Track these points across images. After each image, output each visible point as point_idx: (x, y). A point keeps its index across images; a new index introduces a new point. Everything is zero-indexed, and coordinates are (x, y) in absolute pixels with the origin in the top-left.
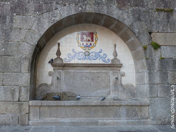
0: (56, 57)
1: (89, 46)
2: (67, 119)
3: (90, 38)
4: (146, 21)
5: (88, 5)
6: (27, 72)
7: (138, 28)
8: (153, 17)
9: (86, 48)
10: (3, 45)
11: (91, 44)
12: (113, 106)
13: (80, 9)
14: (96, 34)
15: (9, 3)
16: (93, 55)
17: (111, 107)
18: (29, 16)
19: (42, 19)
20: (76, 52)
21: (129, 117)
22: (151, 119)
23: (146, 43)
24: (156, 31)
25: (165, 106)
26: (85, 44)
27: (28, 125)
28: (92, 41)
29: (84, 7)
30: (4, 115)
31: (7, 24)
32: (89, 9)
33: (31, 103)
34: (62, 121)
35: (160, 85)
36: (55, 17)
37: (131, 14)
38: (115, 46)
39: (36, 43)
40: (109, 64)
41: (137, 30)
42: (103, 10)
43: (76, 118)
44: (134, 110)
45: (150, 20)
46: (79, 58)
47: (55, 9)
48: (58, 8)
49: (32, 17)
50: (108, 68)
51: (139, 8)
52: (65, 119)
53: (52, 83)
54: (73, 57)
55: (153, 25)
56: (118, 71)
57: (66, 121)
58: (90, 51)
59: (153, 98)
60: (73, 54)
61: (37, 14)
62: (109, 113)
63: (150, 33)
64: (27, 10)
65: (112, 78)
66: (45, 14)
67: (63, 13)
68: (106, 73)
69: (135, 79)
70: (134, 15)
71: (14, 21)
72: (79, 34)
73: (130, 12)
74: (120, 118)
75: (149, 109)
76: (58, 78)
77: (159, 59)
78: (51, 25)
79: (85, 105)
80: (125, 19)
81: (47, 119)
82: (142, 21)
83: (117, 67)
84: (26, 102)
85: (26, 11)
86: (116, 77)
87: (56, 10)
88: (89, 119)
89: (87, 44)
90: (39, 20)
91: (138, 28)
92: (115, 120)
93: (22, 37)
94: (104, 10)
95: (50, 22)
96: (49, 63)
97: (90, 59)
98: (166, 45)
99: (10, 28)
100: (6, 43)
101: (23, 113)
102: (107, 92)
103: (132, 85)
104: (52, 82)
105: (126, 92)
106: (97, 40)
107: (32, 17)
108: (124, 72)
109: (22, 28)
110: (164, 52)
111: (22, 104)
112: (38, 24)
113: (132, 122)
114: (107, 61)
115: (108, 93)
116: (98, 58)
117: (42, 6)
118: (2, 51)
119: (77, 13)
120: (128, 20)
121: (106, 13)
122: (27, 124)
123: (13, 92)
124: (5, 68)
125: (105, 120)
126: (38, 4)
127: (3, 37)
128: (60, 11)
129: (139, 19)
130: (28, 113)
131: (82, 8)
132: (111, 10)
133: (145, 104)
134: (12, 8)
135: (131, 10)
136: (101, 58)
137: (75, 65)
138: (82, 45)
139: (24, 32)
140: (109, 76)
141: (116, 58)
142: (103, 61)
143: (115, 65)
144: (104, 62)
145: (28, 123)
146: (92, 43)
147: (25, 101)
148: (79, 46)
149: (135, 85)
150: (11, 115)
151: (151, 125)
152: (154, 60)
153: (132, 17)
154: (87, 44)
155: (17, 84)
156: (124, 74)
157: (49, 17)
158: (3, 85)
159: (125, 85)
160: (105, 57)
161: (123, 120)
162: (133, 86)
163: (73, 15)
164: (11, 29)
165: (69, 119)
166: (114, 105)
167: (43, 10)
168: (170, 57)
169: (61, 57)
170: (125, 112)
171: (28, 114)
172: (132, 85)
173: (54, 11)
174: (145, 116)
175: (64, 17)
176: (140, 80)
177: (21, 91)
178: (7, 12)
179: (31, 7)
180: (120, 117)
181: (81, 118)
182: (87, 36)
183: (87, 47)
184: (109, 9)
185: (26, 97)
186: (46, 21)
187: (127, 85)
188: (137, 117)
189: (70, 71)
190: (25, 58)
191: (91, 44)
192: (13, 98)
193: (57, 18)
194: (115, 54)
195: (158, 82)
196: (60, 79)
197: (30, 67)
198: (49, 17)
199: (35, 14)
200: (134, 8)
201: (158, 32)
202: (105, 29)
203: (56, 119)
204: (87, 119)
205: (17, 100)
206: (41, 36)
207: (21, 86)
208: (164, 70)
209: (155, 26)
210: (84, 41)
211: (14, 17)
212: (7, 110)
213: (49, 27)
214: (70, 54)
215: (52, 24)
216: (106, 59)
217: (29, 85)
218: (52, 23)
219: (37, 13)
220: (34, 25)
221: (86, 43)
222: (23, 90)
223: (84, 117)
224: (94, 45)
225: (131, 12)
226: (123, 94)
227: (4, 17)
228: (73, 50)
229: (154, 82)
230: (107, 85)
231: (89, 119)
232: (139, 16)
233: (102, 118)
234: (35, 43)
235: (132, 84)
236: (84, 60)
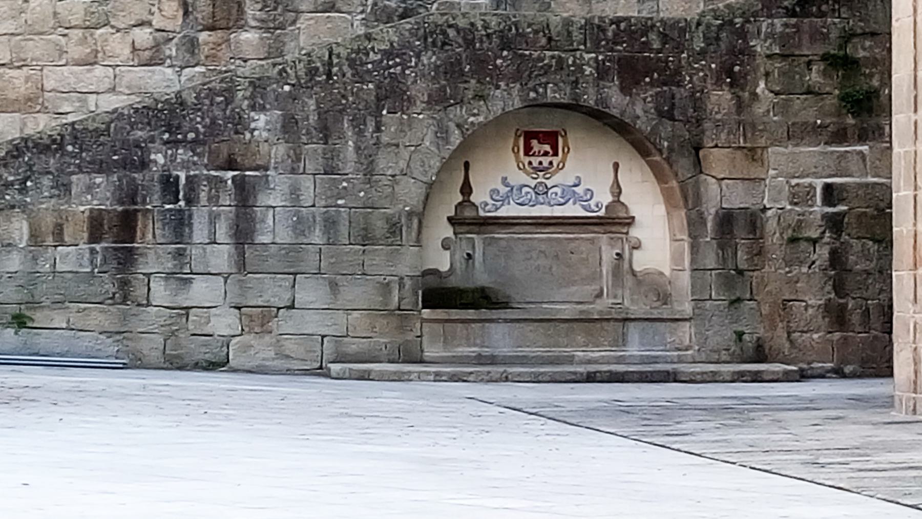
0: (460, 198)
5: (551, 85)
11: (551, 163)
12: (608, 320)
13: (532, 95)
14: (566, 134)
15: (371, 86)
16: (556, 194)
17: (605, 324)
20: (512, 184)
24: (711, 145)
28: (553, 155)
29: (541, 90)
33: (426, 313)
36: (474, 115)
37: (651, 105)
38: (616, 166)
41: (666, 144)
50: (596, 229)
54: (505, 200)
56: (624, 236)
58: (549, 183)
60: (504, 190)
65: (608, 255)
68: (592, 241)
69: (668, 256)
72: (520, 136)
73: (649, 99)
76: (468, 255)
80: (638, 117)
81: (460, 349)
83: (620, 224)
85: (409, 101)
86: (618, 251)
89: (541, 163)
96: (735, 332)
102: (595, 290)
103: (661, 274)
105: (642, 290)
107: (422, 117)
108: (639, 237)
116: (571, 201)
123: (386, 288)
131: (537, 92)
135: (651, 96)
136: (578, 199)
137: (511, 221)
140: (600, 248)
141: (619, 201)
143: (616, 221)
146: (556, 161)
149: (667, 273)
154: (541, 163)
156: (640, 243)
160: (589, 197)
164: (377, 144)
168: (742, 206)
169: (472, 198)
176: (676, 258)
182: (540, 143)
187: (647, 273)
189: (496, 236)
191: (551, 163)
194: (617, 190)
201: (716, 146)
210: (533, 155)
211: (383, 119)
214: (495, 191)
216: (592, 203)
228: (504, 180)
236: (533, 206)
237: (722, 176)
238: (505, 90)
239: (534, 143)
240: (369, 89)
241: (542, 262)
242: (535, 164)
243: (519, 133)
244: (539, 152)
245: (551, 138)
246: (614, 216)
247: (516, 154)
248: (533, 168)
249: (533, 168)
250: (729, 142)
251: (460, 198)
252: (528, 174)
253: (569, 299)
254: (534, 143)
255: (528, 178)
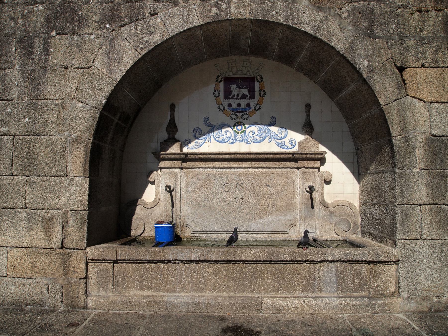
0: (166, 136)
1: (245, 109)
2: (182, 294)
3: (245, 91)
4: (389, 38)
6: (82, 175)
7: (369, 56)
8: (407, 26)
9: (238, 114)
10: (25, 109)
11: (248, 105)
15: (41, 7)
16: (254, 132)
17: (297, 266)
18: (86, 36)
19: (118, 41)
21: (344, 292)
22: (403, 299)
23: (388, 96)
25: (440, 264)
26: (234, 106)
27: (85, 307)
29: (224, 6)
30: (30, 280)
31: (36, 57)
32: (236, 11)
34: (171, 300)
35: (427, 207)
36: (150, 34)
37: (348, 21)
38: (308, 107)
39: (104, 102)
40: (293, 154)
41: (366, 63)
42: (274, 12)
43: (206, 292)
44: (358, 274)
45: (399, 35)
46: (221, 138)
47: (152, 15)
48: (158, 11)
49: (93, 36)
51: (369, 4)
52: (177, 294)
53: (155, 198)
55: (407, 49)
57: (179, 300)
59: (409, 242)
61: (108, 29)
62: (291, 282)
63: (401, 69)
64: (82, 22)
66: (126, 27)
67: (172, 23)
68: (286, 176)
70: (355, 23)
71: (52, 50)
72: (220, 82)
73: (345, 15)
74: (320, 294)
75: (397, 271)
77: (426, 139)
78: (139, 54)
79: (226, 259)
80: (334, 34)
81: (132, 293)
82: (380, 38)
84: (80, 252)
87: (152, 18)
88: (239, 295)
89: (239, 105)
90: (112, 42)
91: (367, 57)
92: (307, 301)
93: (70, 87)
94: (277, 13)
95: (138, 46)
97: (248, 143)
98: (443, 100)
99: (42, 67)
100: (32, 105)
101: (74, 278)
104: (156, 196)
106: (264, 96)
109: (70, 65)
110: (438, 119)
111: (69, 256)
112: (109, 54)
113: (353, 305)
114: (287, 144)
115: (291, 223)
116: (267, 138)
117: (118, 10)
118: (23, 125)
119: (205, 21)
120: (342, 35)
121: (281, 19)
122: (82, 304)
124: (29, 166)
125: (280, 300)
126: (110, 5)
127: (26, 91)
128: (164, 20)
129: (370, 34)
130: (84, 278)
131: (220, 9)
132: (294, 11)
133: (389, 259)
134: (47, 20)
138: (226, 108)
139: (73, 74)
142: (279, 145)
144: (281, 147)
145: (85, 303)
146: (253, 103)
147: (77, 249)
148: (220, 110)
150: (46, 282)
151: (402, 312)
152: (413, 140)
153: (350, 28)
154: (239, 105)
155: (59, 206)
157: (136, 35)
158: (26, 208)
159: (332, 203)
160: (283, 135)
161: (327, 300)
162: (353, 205)
163: (196, 28)
165: (186, 294)
166: (305, 261)
167: (121, 18)
170: (333, 279)
171: (85, 280)
172: (350, 204)
173: (148, 21)
174: (387, 288)
175: (173, 34)
177: (67, 222)
178: (37, 29)
179: (92, 12)
180: (321, 291)
181: (219, 292)
182: (238, 87)
183: (239, 112)
184: (291, 9)
185: (78, 238)
186: (128, 46)
188: (364, 291)
190: (77, 140)
191: (248, 105)
192: (48, 241)
193: (156, 36)
195: (424, 199)
196: (174, 189)
197: (88, 162)
198: (136, 35)
199: (101, 31)
200: (356, 4)
201: (423, 66)
202: (285, 68)
203: (155, 294)
204: (232, 294)
205: (58, 244)
206: (116, 83)
207: (68, 209)
208: (439, 167)
209: (412, 51)
210: (232, 98)
212: (35, 269)
213: (136, 59)
215: (143, 53)
217: (86, 207)
218: (142, 49)
219: (108, 26)
220: (98, 59)
221: (246, 103)
222: (72, 218)
223: (224, 291)
224: (255, 106)
225: (348, 16)
226: (328, 227)
227: (28, 40)
229: (412, 200)
230: (288, 204)
231: (239, 295)
232: (371, 25)
233: (273, 294)
234: (101, 102)
235: (351, 201)
236: (233, 143)
237: (430, 98)
238: (183, 8)
239: (233, 87)
240: (39, 11)
241: (239, 194)
242: (234, 106)
243: (220, 79)
244: (238, 95)
245: (249, 82)
246: (307, 151)
247: (217, 97)
248: (233, 110)
249: (233, 110)
250: (437, 62)
251: (166, 136)
252: (228, 115)
253: (266, 228)
254: (233, 87)
255: (229, 119)
